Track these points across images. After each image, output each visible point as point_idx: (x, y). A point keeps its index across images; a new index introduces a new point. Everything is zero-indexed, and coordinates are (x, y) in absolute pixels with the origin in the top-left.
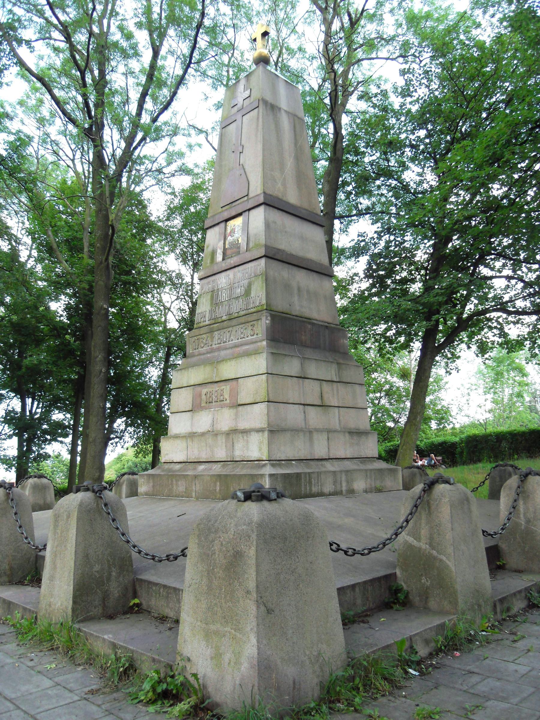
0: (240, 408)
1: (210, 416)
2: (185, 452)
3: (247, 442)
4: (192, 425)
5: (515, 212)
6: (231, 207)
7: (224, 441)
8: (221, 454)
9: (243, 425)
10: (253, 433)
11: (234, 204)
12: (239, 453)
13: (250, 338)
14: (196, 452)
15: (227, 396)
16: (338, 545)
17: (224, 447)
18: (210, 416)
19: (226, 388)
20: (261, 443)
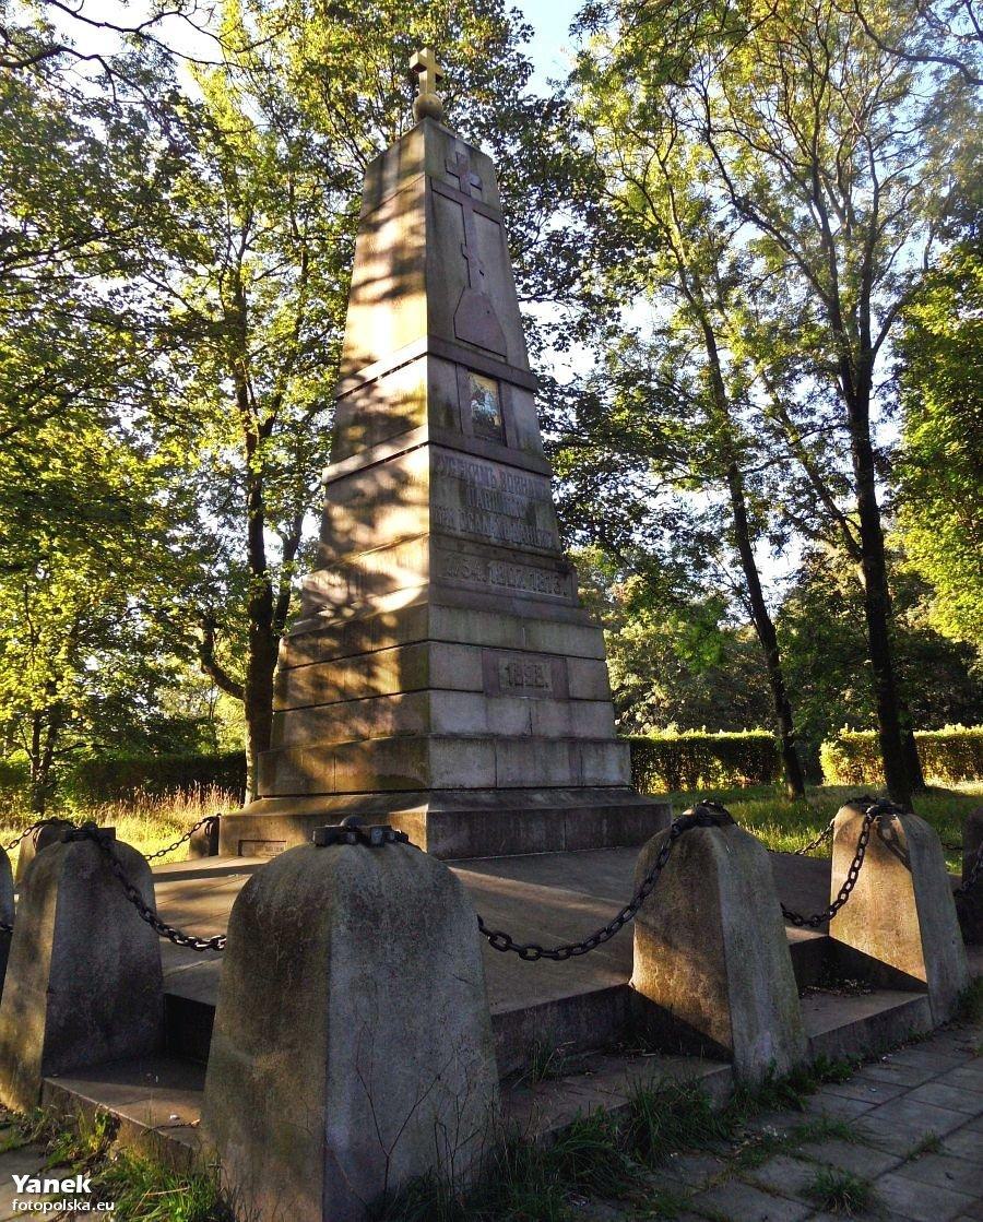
0: (575, 705)
1: (523, 708)
2: (492, 770)
3: (603, 757)
4: (488, 720)
5: (128, 320)
6: (475, 353)
7: (566, 753)
8: (561, 774)
9: (582, 731)
10: (610, 745)
11: (481, 352)
12: (590, 774)
13: (553, 595)
14: (515, 770)
15: (548, 680)
16: (508, 939)
17: (567, 764)
18: (523, 708)
19: (546, 667)
20: (622, 760)
